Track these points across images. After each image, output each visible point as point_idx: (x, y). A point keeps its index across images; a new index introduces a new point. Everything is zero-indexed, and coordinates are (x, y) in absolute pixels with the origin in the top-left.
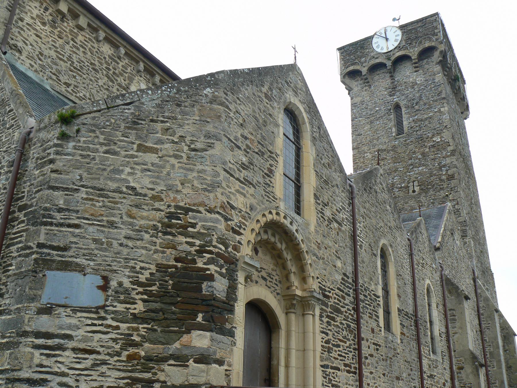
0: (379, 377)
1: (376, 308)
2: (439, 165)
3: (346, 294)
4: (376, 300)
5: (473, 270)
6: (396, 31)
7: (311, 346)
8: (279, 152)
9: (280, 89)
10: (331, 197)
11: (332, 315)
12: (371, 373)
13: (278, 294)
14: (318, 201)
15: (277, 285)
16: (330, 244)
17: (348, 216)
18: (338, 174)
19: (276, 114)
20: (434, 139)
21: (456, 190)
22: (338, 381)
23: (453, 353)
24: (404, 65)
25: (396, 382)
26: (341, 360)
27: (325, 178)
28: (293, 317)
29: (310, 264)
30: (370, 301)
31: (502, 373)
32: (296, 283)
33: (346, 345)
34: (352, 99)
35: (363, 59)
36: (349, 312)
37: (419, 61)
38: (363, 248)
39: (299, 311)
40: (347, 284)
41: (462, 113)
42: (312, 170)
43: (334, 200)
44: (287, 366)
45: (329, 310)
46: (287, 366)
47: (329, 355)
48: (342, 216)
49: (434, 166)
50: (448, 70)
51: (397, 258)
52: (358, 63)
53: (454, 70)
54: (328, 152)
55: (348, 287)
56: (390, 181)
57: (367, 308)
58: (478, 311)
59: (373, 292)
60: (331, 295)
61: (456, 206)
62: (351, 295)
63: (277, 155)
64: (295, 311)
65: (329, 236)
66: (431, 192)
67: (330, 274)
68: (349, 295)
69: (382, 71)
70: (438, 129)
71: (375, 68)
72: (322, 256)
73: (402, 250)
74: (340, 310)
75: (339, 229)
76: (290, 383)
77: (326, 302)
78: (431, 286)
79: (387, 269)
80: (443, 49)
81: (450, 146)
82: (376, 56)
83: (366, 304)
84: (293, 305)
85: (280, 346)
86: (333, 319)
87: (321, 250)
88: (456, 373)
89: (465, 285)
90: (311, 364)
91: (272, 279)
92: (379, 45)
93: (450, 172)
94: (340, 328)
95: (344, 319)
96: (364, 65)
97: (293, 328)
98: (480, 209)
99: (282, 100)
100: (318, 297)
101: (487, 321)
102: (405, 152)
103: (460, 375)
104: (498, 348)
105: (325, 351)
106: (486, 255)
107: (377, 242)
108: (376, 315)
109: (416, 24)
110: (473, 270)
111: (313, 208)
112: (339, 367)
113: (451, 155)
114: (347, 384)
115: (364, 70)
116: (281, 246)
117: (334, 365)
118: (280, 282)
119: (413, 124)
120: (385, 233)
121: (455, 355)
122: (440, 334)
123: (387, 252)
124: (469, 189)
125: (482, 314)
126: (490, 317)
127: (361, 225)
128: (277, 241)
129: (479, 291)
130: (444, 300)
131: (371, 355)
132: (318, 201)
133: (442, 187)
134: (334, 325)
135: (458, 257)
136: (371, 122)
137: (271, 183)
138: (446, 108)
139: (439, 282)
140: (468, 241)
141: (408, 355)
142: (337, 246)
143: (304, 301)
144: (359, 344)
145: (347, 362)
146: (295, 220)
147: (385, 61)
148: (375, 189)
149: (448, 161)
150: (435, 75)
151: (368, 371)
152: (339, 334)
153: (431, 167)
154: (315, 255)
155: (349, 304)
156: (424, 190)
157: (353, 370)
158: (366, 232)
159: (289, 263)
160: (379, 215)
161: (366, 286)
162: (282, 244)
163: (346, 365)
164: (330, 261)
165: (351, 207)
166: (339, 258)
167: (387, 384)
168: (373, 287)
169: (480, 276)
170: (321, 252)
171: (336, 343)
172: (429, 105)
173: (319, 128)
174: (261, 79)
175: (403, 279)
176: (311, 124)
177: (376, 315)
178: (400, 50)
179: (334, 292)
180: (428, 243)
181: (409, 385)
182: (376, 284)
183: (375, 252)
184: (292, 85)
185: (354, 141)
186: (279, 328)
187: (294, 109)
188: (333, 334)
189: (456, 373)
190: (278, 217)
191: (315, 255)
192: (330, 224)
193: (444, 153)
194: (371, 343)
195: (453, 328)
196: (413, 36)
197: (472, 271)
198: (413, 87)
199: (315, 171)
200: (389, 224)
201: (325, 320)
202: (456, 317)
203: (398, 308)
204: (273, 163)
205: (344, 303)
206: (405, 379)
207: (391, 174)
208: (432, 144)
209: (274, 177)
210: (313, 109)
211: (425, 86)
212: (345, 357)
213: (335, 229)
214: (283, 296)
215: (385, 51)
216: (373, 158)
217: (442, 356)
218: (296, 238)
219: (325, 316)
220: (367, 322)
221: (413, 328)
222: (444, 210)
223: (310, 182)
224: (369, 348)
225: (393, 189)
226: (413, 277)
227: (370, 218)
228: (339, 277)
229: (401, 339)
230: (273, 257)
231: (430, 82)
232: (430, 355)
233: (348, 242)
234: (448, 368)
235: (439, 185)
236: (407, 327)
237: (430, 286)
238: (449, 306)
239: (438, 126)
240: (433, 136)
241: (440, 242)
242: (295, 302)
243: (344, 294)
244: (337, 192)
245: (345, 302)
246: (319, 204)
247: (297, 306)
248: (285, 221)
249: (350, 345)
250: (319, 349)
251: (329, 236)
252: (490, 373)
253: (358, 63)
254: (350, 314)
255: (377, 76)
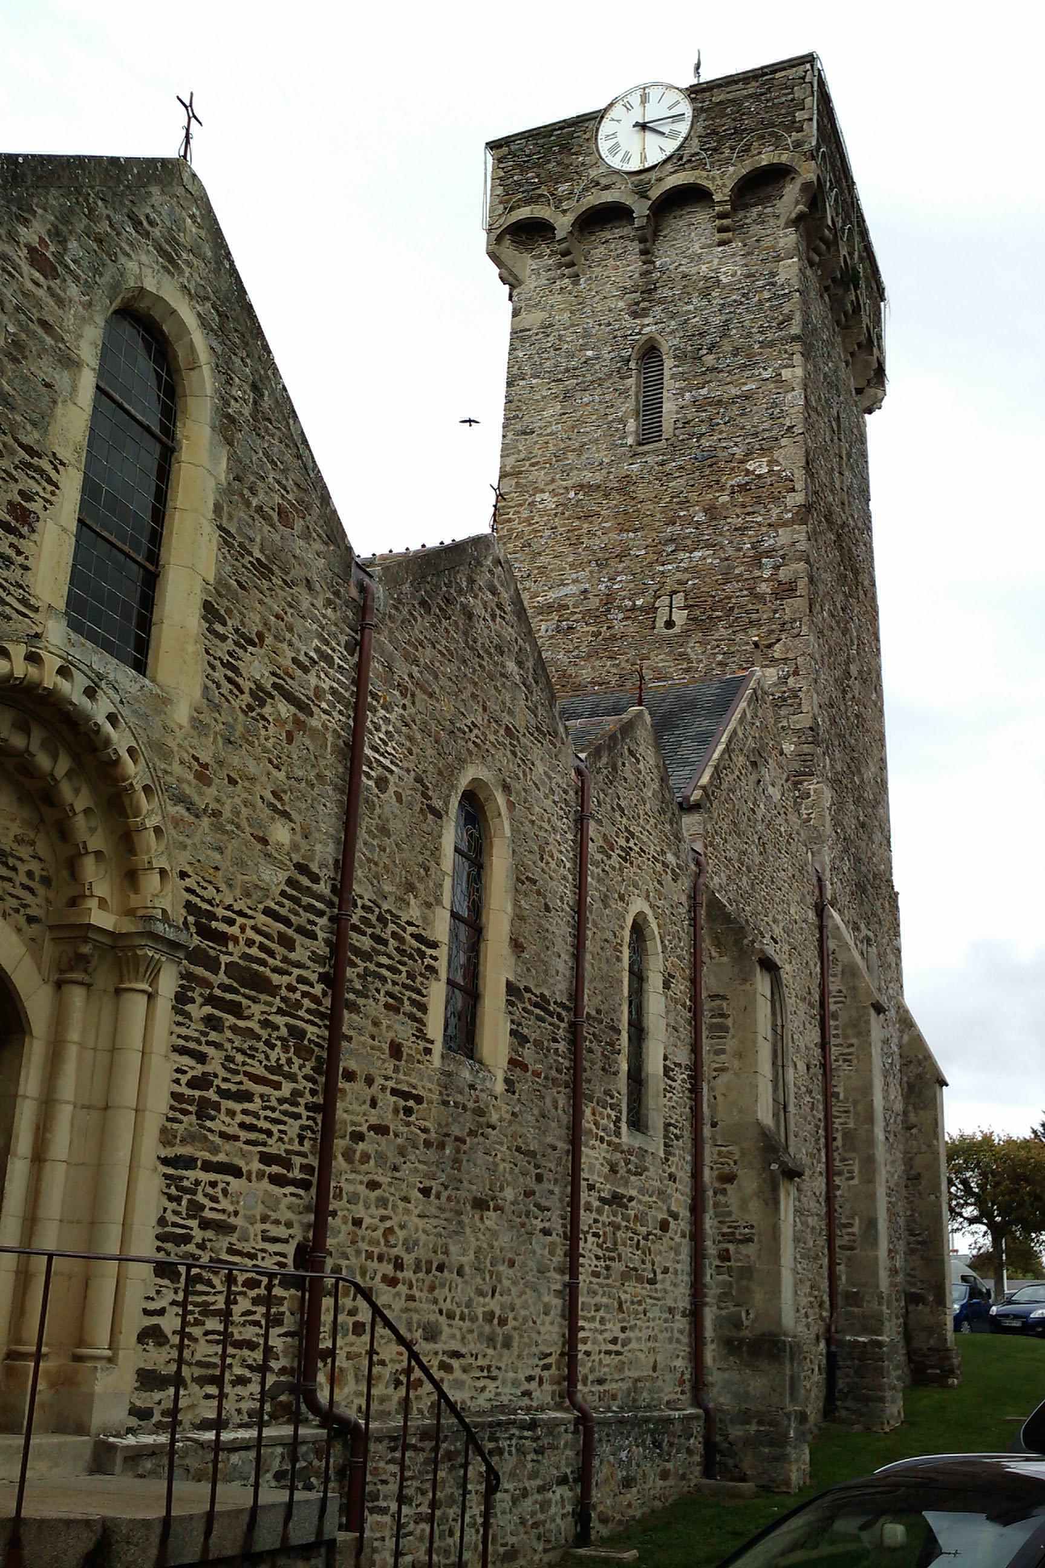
0: (406, 1199)
1: (419, 979)
2: (753, 548)
3: (300, 930)
4: (422, 955)
5: (820, 880)
6: (678, 103)
7: (128, 1095)
8: (64, 454)
9: (100, 241)
10: (277, 617)
11: (229, 996)
12: (373, 1185)
13: (31, 920)
14: (218, 627)
15: (32, 891)
16: (253, 768)
17: (339, 682)
18: (318, 546)
19: (70, 321)
20: (750, 466)
21: (796, 631)
22: (231, 1209)
23: (707, 1131)
24: (687, 219)
25: (470, 1216)
26: (248, 1142)
27: (257, 554)
28: (77, 997)
29: (158, 830)
30: (398, 957)
31: (872, 1197)
32: (101, 889)
33: (277, 1094)
34: (516, 313)
35: (563, 188)
36: (306, 988)
37: (735, 209)
38: (392, 789)
39: (103, 978)
40: (306, 900)
41: (859, 391)
42: (205, 523)
43: (290, 629)
44: (39, 1158)
45: (222, 977)
46: (39, 1158)
47: (202, 1126)
48: (314, 681)
49: (740, 550)
50: (823, 247)
51: (527, 827)
52: (547, 196)
53: (844, 252)
54: (283, 471)
55: (309, 908)
56: (602, 587)
57: (384, 980)
58: (823, 1004)
59: (410, 929)
60: (234, 930)
61: (791, 681)
62: (321, 935)
63: (57, 463)
64: (87, 979)
65: (251, 744)
66: (722, 631)
67: (240, 863)
68: (313, 936)
69: (618, 232)
70: (767, 435)
71: (601, 218)
72: (214, 805)
73: (549, 802)
74: (268, 981)
75: (299, 724)
76: (41, 1213)
77: (212, 952)
78: (651, 918)
79: (485, 859)
80: (812, 177)
81: (793, 490)
82: (604, 182)
83: (379, 965)
84: (80, 961)
85: (21, 1092)
86: (236, 1010)
87: (209, 785)
88: (710, 1193)
89: (782, 924)
90: (123, 1154)
91: (14, 869)
92: (617, 145)
93: (783, 574)
94: (259, 1038)
95: (280, 1012)
96: (565, 205)
97: (74, 1035)
98: (880, 697)
99: (105, 279)
100: (171, 937)
101: (846, 1037)
102: (657, 499)
103: (721, 1198)
104: (870, 1120)
105: (185, 1112)
106: (878, 837)
107: (447, 774)
108: (413, 1002)
109: (741, 85)
110: (820, 880)
111: (194, 649)
112: (241, 1163)
113: (793, 521)
114: (264, 1219)
115: (563, 224)
116: (57, 766)
117: (221, 1158)
118: (46, 881)
119: (691, 413)
120: (488, 746)
121: (713, 1138)
122: (667, 1070)
123: (489, 808)
124: (845, 632)
125: (835, 1016)
126: (855, 1026)
127: (392, 717)
128: (34, 747)
129: (831, 944)
130: (696, 965)
131: (381, 1130)
132: (218, 627)
133: (754, 616)
134: (234, 1029)
135: (768, 835)
136: (567, 396)
137: (19, 553)
138: (799, 372)
139: (683, 910)
140: (815, 791)
141: (530, 1133)
142: (281, 775)
143: (123, 948)
144: (331, 1093)
145: (274, 1147)
146: (109, 683)
147: (629, 200)
148: (464, 607)
149: (784, 536)
150: (778, 259)
151: (359, 1177)
152: (253, 1057)
153: (730, 552)
154: (181, 799)
155: (309, 963)
156: (700, 624)
157: (296, 1174)
158: (410, 739)
159: (80, 823)
160: (471, 688)
161: (385, 907)
162: (55, 758)
163: (267, 1159)
164: (244, 824)
165: (356, 655)
166: (285, 815)
167: (434, 1222)
168: (414, 912)
169: (844, 900)
170: (212, 792)
171: (234, 1088)
172: (749, 356)
173: (255, 387)
174: (20, 198)
175: (538, 893)
176: (225, 372)
177: (413, 1002)
178: (681, 168)
179: (252, 922)
180: (656, 786)
181: (523, 1225)
182: (428, 905)
183: (438, 804)
184: (156, 232)
185: (506, 451)
186: (24, 1033)
187: (156, 314)
188: (229, 1059)
189: (710, 1193)
190: (33, 671)
191: (181, 799)
192: (262, 704)
193: (775, 512)
194: (383, 1089)
195: (718, 1052)
196: (726, 125)
197: (814, 880)
198: (705, 294)
199: (220, 527)
200: (506, 719)
201: (198, 1011)
202: (729, 1022)
203: (509, 984)
204: (36, 488)
205: (285, 960)
206: (509, 1208)
207: (607, 565)
208: (741, 479)
209: (35, 537)
210: (236, 320)
211: (744, 295)
212: (269, 1133)
213: (280, 722)
214: (51, 928)
215: (634, 165)
216: (561, 508)
217: (666, 1137)
218: (107, 742)
219: (199, 1000)
220: (376, 1024)
221: (562, 1047)
222: (738, 688)
223: (192, 560)
224: (374, 1104)
225: (608, 610)
226: (581, 887)
227: (431, 695)
228: (274, 878)
229: (507, 1081)
230: (24, 797)
231: (760, 283)
232: (618, 1134)
233: (331, 766)
234: (684, 1175)
235: (746, 612)
236: (538, 1044)
237: (645, 919)
238: (710, 982)
239: (766, 425)
240: (749, 455)
241: (703, 788)
242: (86, 949)
243: (290, 932)
244: (305, 605)
245: (293, 956)
246: (223, 638)
247: (94, 961)
248: (65, 686)
249: (296, 1093)
250: (159, 1103)
251: (251, 744)
252: (838, 1193)
253: (547, 196)
254: (305, 994)
255: (602, 249)
